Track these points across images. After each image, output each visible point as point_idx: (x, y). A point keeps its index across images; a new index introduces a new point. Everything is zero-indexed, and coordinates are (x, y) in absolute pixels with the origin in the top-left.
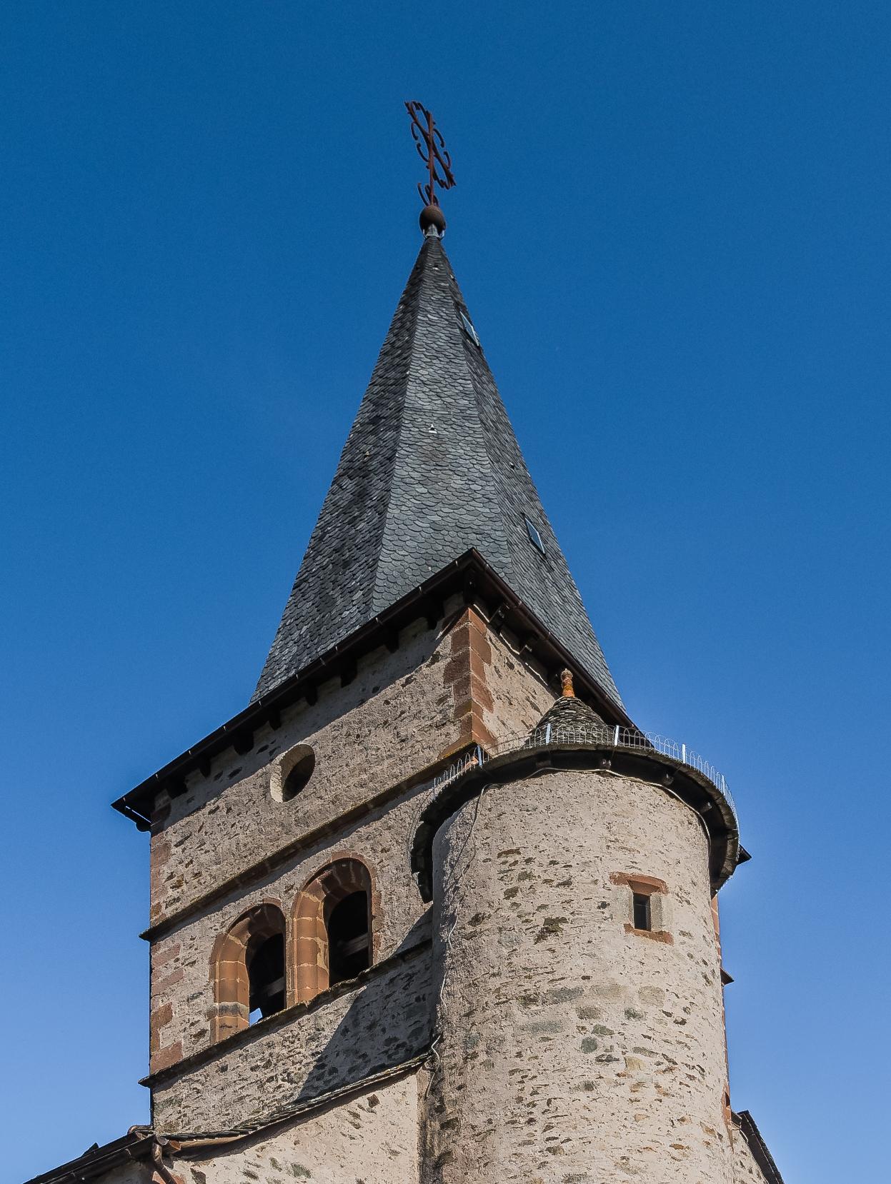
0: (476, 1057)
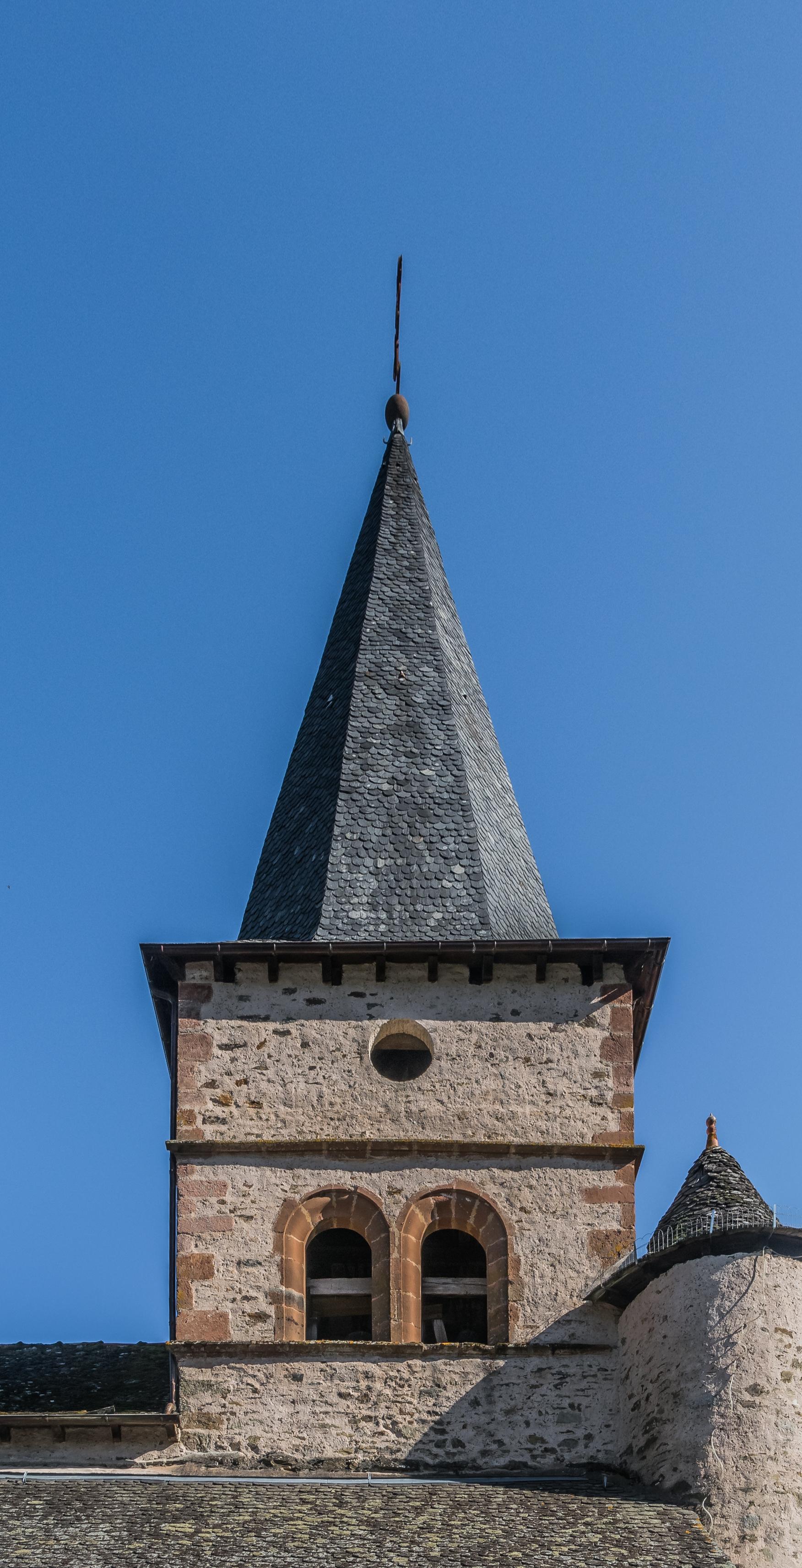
0: (755, 1541)
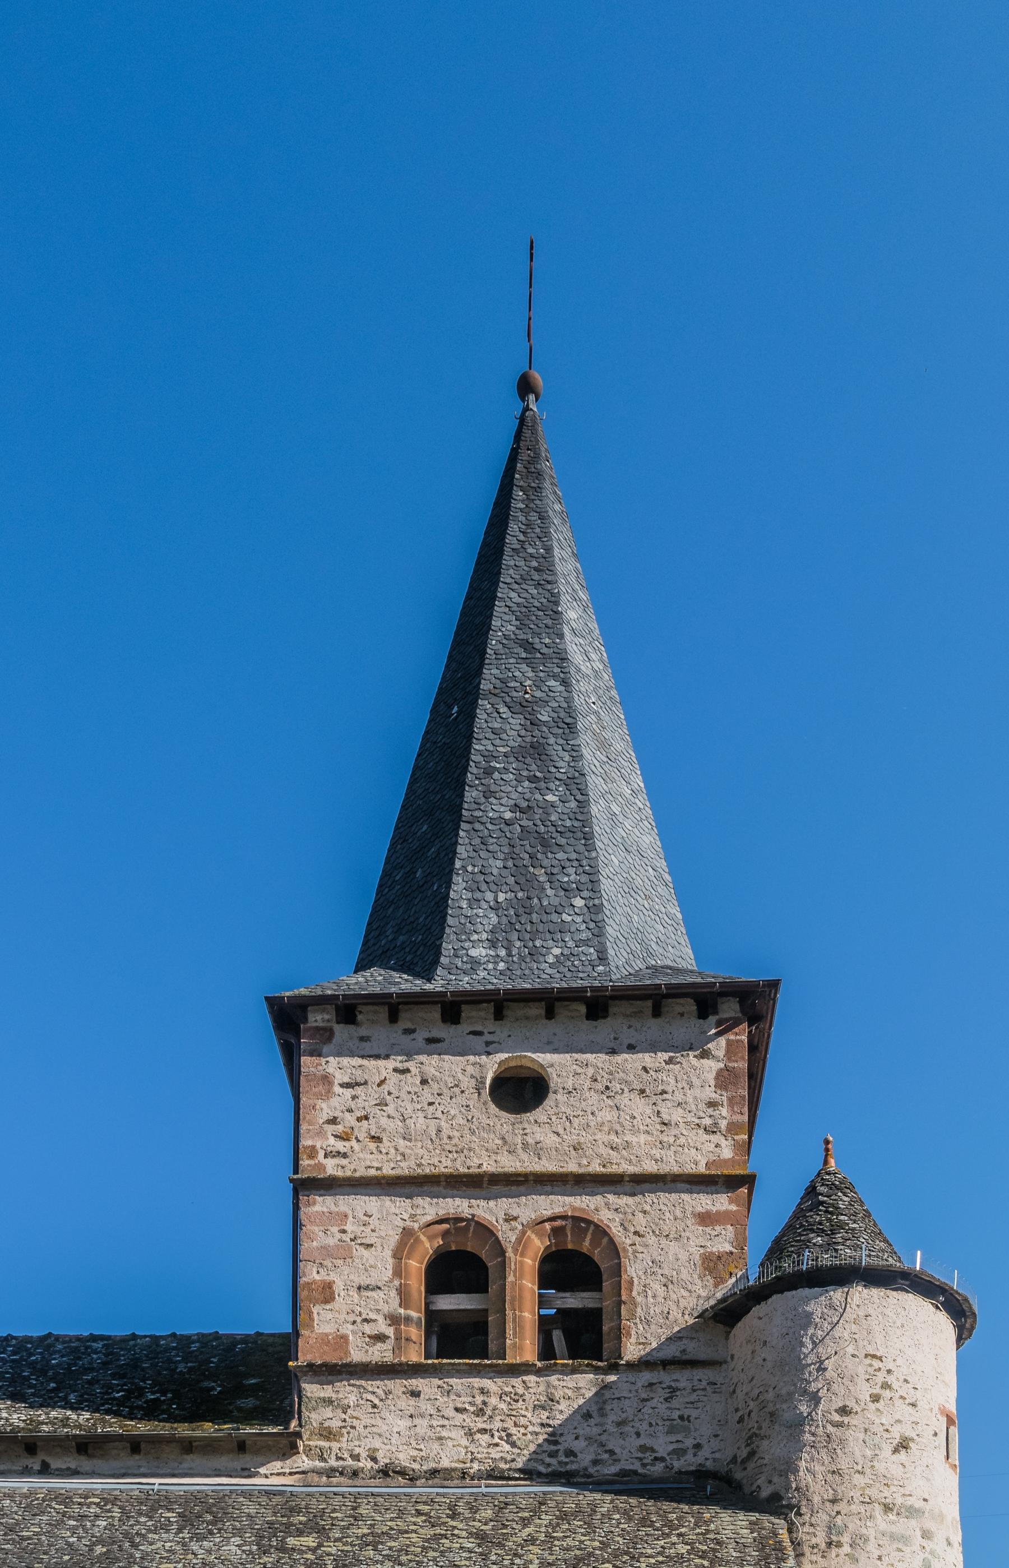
0: (841, 1547)
